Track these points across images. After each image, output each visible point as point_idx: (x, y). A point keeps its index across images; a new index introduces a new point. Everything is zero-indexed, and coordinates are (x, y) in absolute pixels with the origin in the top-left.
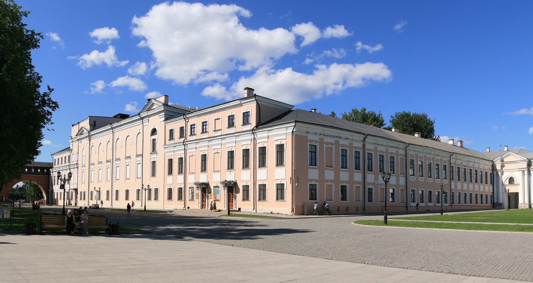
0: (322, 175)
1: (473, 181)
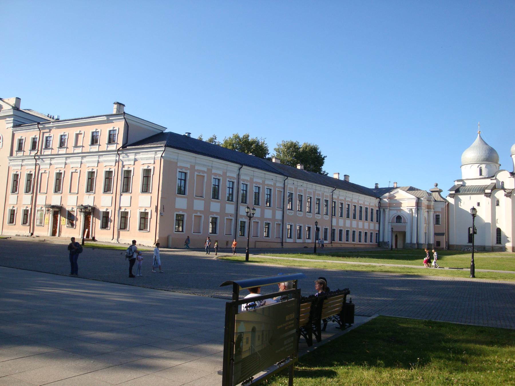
0: (190, 204)
1: (374, 220)
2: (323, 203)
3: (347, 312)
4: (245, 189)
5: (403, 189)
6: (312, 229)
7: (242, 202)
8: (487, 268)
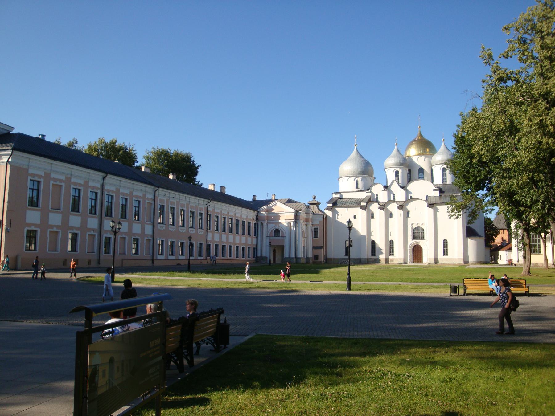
0: (45, 218)
1: (239, 232)
2: (197, 216)
3: (222, 333)
4: (110, 201)
5: (281, 201)
6: (185, 245)
7: (107, 215)
8: (362, 280)
